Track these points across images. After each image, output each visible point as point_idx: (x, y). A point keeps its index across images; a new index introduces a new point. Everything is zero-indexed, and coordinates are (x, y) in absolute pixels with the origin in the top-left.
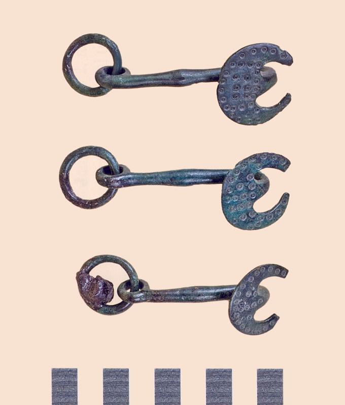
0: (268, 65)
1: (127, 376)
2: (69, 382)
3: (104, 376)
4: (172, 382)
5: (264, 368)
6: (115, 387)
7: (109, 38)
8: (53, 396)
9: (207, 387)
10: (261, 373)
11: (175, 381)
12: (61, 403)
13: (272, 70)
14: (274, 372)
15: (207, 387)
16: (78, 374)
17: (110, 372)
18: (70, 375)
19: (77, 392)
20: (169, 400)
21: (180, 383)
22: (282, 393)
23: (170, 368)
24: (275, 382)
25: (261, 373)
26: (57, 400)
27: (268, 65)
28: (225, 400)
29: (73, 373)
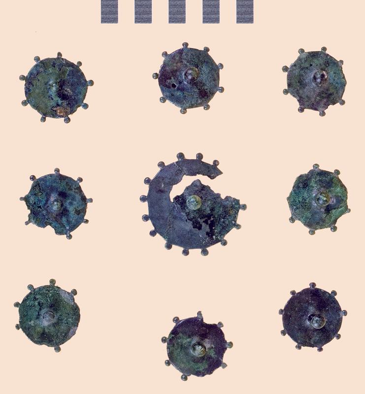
0: (172, 200)
1: (238, 18)
2: (208, 14)
3: (117, 18)
4: (242, 14)
5: (113, 24)
7: (228, 234)
8: (253, 5)
10: (217, 20)
13: (174, 199)
15: (219, 12)
16: (100, 20)
22: (237, 7)
23: (108, 24)
24: (140, 14)
25: (149, 20)
26: (115, 3)
27: (172, 200)
28: (206, 3)
29: (206, 20)
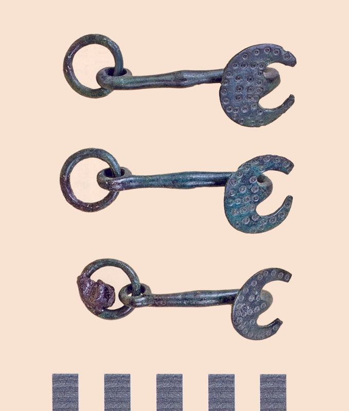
0: (271, 66)
1: (129, 382)
2: (70, 387)
3: (105, 382)
4: (174, 388)
5: (267, 373)
6: (116, 393)
7: (110, 38)
8: (54, 402)
9: (210, 392)
10: (264, 379)
11: (177, 386)
12: (62, 409)
13: (275, 71)
14: (277, 378)
15: (210, 392)
16: (79, 379)
17: (111, 378)
18: (71, 380)
19: (77, 398)
20: (171, 406)
21: (182, 388)
22: (285, 399)
23: (172, 373)
24: (278, 388)
25: (264, 379)
26: (57, 406)
27: (271, 66)
28: (228, 406)
29: (74, 379)
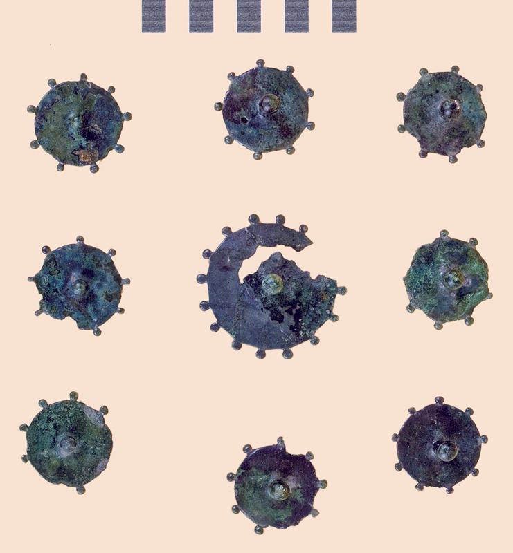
0: (242, 281)
1: (334, 26)
2: (292, 20)
3: (165, 26)
4: (340, 20)
5: (159, 34)
7: (320, 329)
8: (355, 6)
10: (305, 29)
13: (244, 279)
15: (308, 16)
16: (141, 28)
22: (334, 10)
23: (151, 34)
24: (197, 20)
25: (209, 29)
26: (161, 4)
27: (242, 281)
28: (290, 4)
29: (289, 29)
